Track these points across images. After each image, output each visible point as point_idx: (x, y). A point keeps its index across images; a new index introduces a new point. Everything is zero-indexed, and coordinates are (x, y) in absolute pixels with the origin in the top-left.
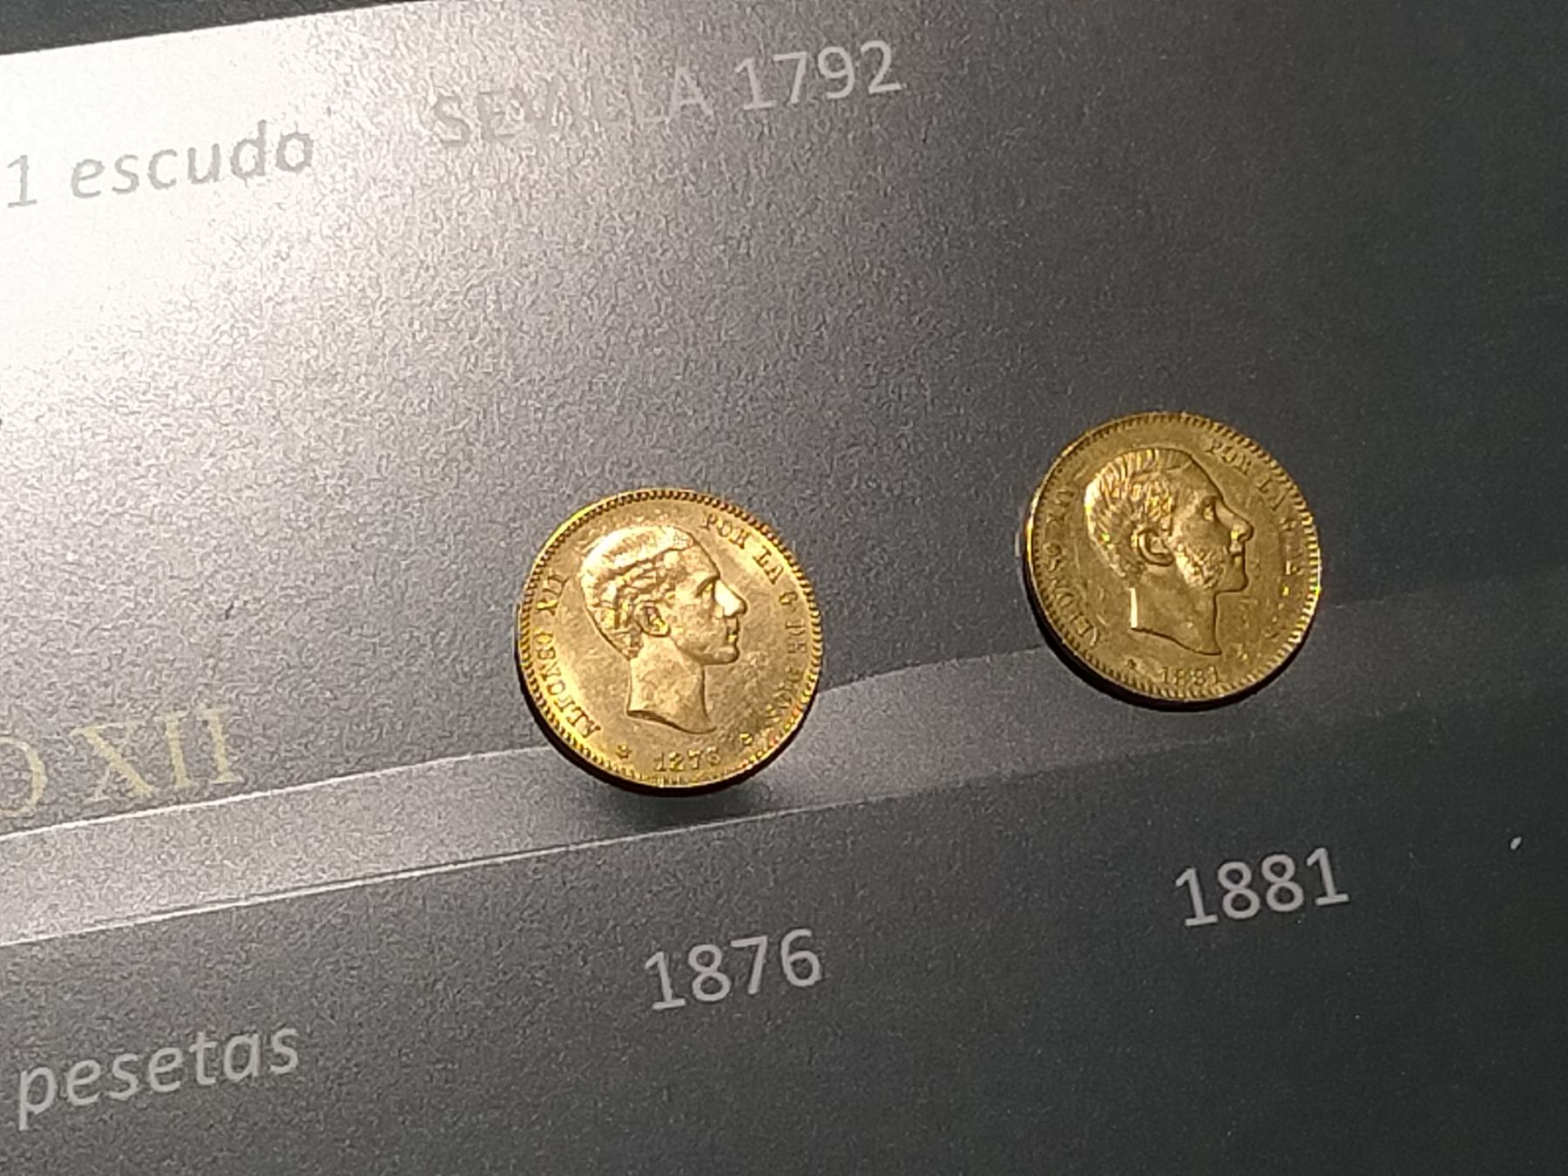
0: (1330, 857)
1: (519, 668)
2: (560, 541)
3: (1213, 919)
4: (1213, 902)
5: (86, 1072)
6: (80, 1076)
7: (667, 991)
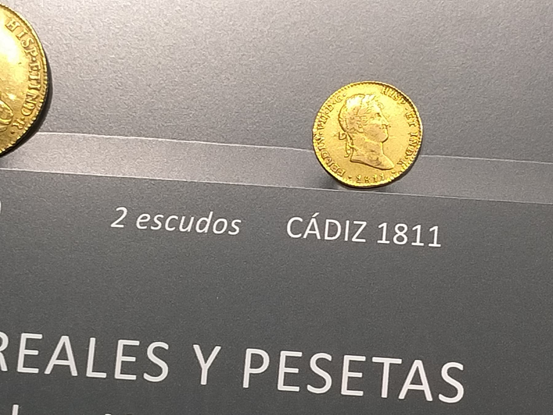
0: (421, 230)
2: (378, 84)
3: (388, 242)
4: (390, 237)
5: (145, 218)
6: (142, 219)
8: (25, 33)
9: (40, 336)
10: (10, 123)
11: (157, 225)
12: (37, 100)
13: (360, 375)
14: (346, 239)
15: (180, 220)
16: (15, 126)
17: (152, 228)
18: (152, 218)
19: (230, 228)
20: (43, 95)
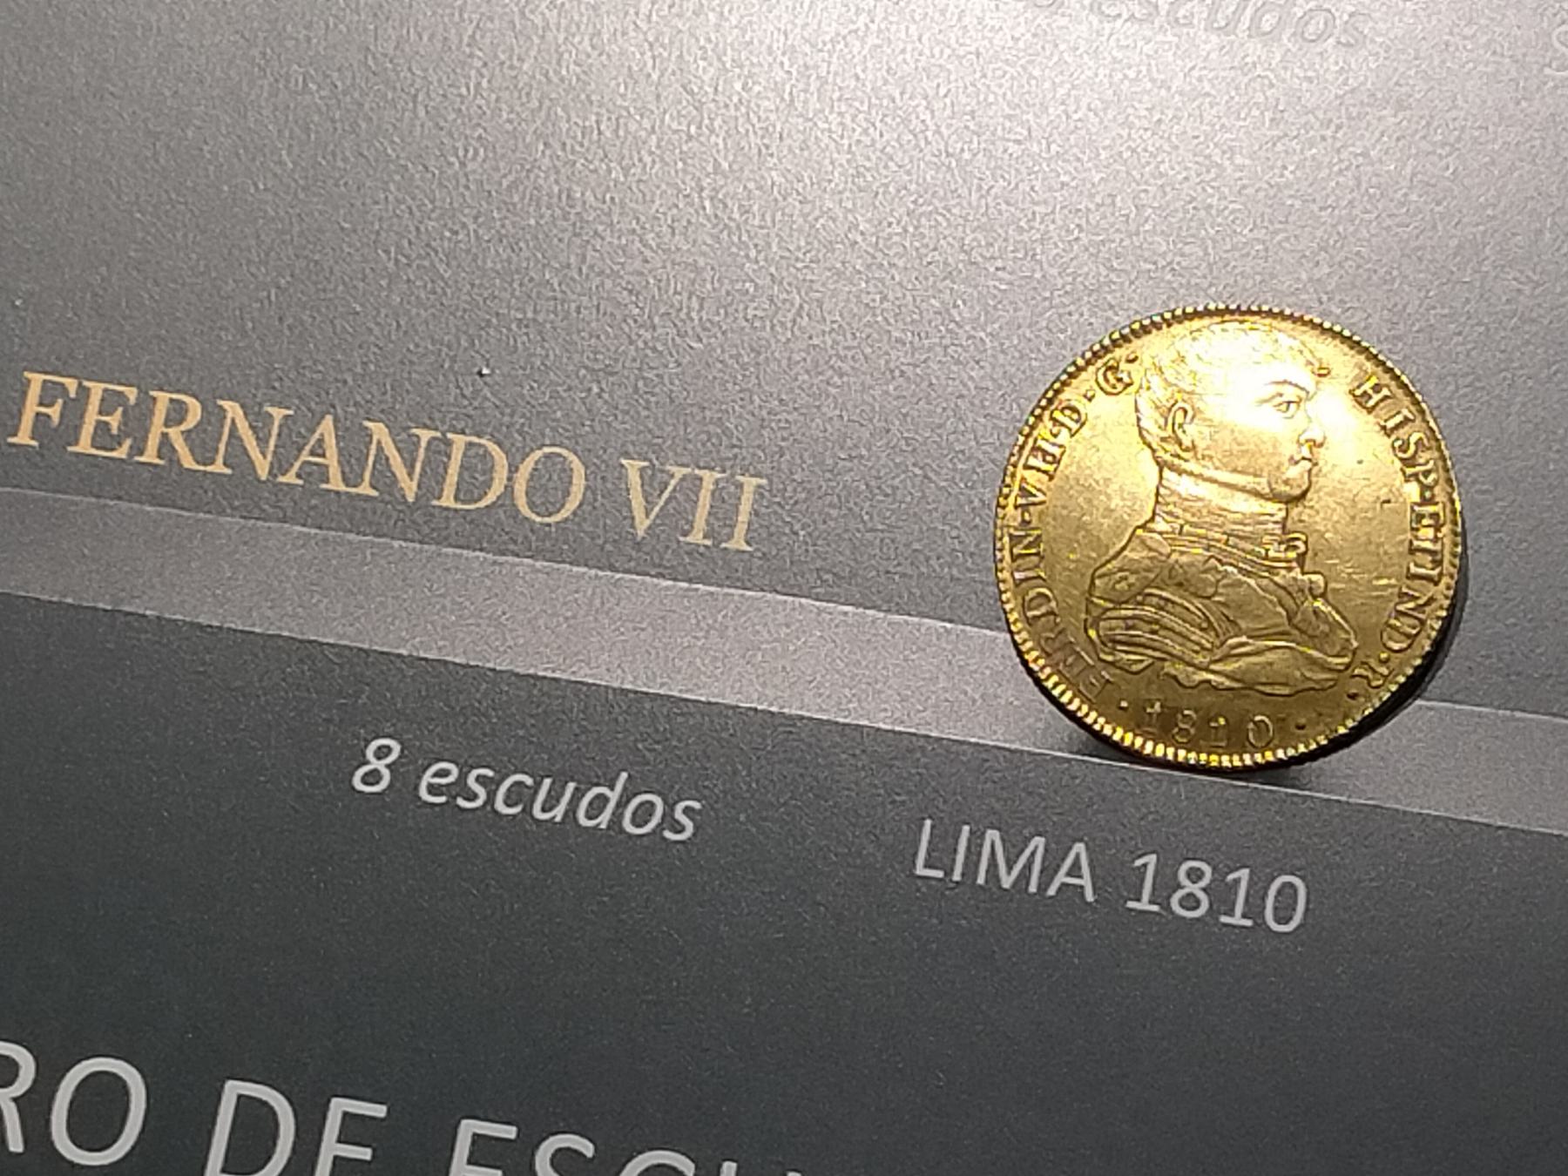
1: (1030, 672)
4: (1162, 894)
5: (443, 773)
6: (436, 775)
7: (1239, 908)
8: (1407, 420)
9: (379, 1111)
10: (1348, 666)
11: (681, 830)
12: (1427, 609)
13: (365, 1154)
14: (1033, 889)
15: (538, 785)
16: (1360, 676)
17: (461, 802)
18: (463, 776)
19: (669, 821)
20: (1446, 597)
